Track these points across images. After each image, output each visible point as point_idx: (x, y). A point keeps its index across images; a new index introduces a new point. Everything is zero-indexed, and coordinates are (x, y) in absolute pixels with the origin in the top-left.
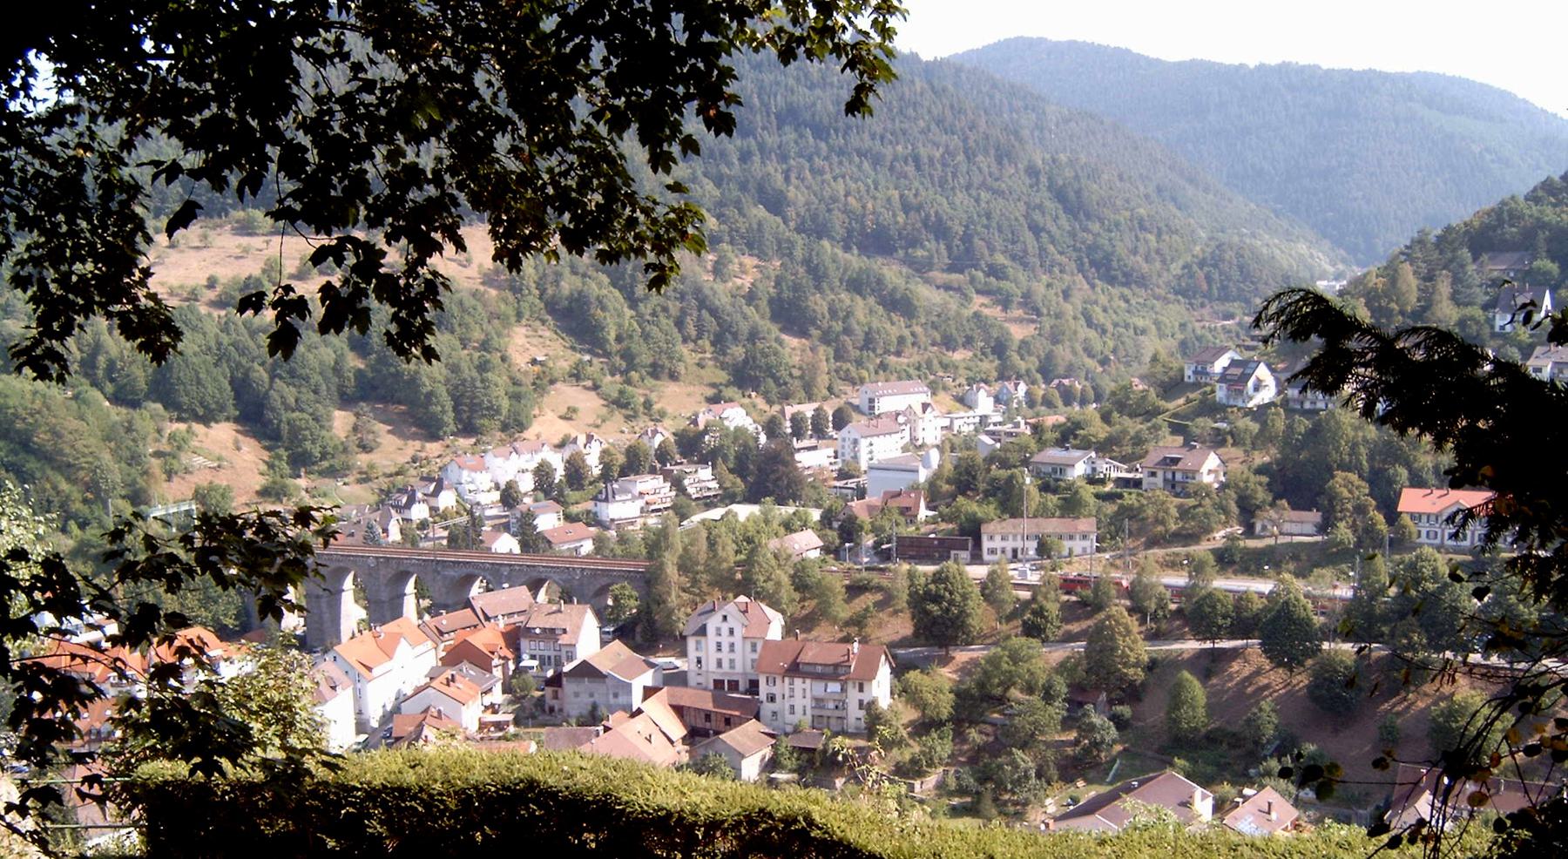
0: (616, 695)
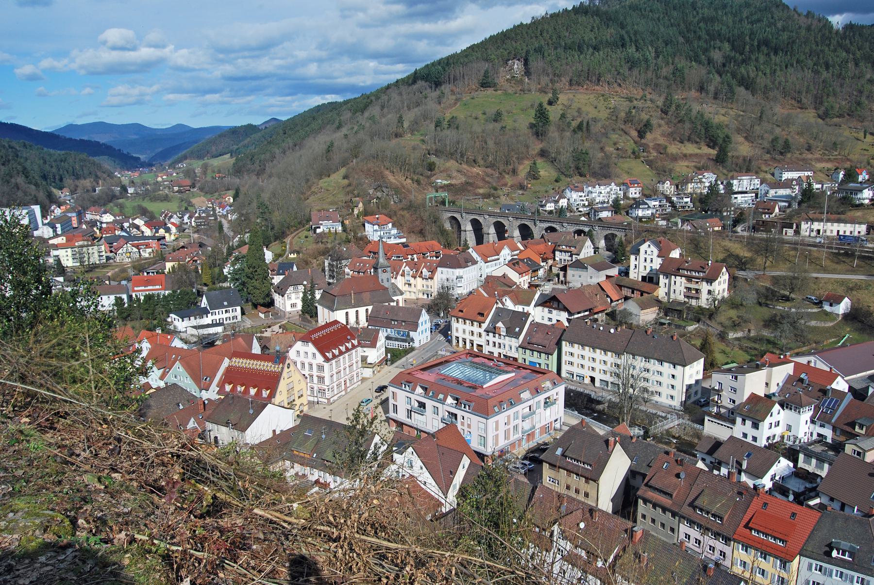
0: (591, 277)
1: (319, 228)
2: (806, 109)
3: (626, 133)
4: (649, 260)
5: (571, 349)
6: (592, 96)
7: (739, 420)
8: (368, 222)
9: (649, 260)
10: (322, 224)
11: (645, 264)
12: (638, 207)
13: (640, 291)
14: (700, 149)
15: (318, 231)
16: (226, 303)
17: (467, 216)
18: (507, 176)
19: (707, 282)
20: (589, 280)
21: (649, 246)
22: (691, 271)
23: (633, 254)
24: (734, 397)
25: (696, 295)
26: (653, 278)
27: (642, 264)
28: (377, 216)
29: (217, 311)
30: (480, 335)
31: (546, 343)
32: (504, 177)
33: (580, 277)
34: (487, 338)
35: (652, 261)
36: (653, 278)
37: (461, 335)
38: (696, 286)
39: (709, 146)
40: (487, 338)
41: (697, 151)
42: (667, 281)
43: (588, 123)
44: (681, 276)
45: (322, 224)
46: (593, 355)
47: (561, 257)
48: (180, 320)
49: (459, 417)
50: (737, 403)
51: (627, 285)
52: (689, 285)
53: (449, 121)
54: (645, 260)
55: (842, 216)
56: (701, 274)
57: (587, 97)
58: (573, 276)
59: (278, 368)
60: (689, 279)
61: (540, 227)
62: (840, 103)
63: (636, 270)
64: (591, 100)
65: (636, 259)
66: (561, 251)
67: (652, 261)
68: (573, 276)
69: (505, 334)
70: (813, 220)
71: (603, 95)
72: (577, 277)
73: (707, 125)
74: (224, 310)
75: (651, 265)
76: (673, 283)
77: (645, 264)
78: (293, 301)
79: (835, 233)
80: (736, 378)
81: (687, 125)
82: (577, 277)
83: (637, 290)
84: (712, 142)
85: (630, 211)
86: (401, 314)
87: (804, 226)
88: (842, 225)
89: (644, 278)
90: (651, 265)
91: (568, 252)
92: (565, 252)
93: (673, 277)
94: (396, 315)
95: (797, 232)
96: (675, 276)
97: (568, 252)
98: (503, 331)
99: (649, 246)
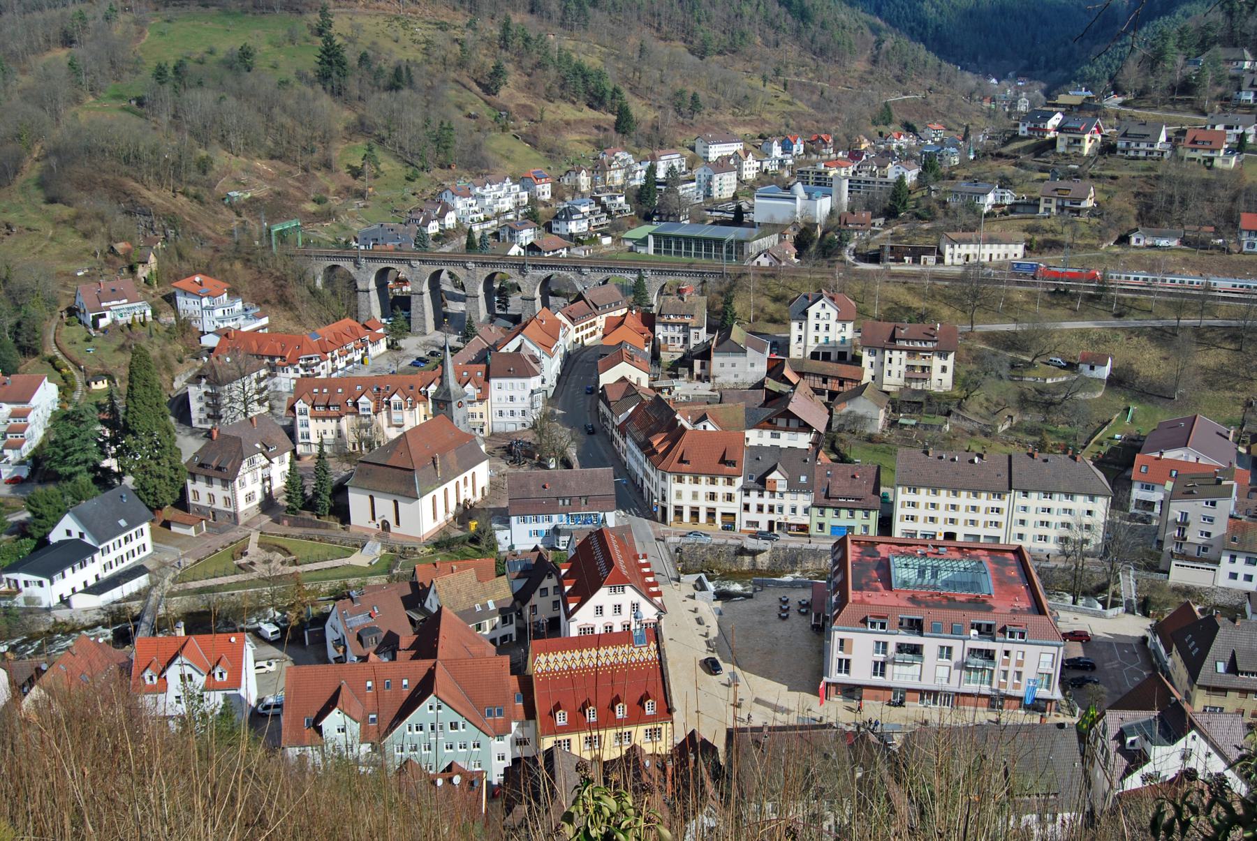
0: (752, 365)
1: (104, 316)
2: (672, 40)
3: (464, 86)
4: (822, 328)
5: (911, 497)
6: (380, 19)
7: (1225, 559)
8: (185, 293)
9: (822, 328)
10: (108, 309)
11: (817, 334)
12: (568, 220)
13: (837, 378)
14: (581, 111)
15: (103, 323)
16: (123, 523)
17: (371, 264)
18: (319, 174)
19: (940, 356)
20: (749, 369)
21: (823, 306)
22: (913, 341)
23: (797, 319)
24: (1207, 528)
25: (924, 376)
26: (829, 354)
27: (812, 333)
28: (197, 279)
29: (110, 543)
30: (730, 497)
31: (858, 493)
32: (314, 177)
33: (733, 365)
34: (746, 500)
35: (827, 328)
36: (829, 354)
37: (687, 503)
38: (924, 363)
39: (590, 106)
40: (746, 500)
41: (579, 115)
42: (873, 359)
43: (407, 69)
44: (901, 350)
45: (108, 309)
46: (934, 499)
47: (666, 334)
48: (46, 581)
49: (999, 656)
50: (1213, 536)
51: (814, 371)
52: (912, 362)
53: (175, 68)
54: (817, 328)
55: (972, 235)
56: (930, 345)
57: (374, 21)
58: (722, 365)
59: (649, 651)
60: (912, 353)
61: (533, 277)
62: (716, 36)
63: (801, 345)
64: (381, 26)
65: (800, 327)
66: (666, 324)
67: (827, 328)
68: (722, 365)
69: (784, 489)
70: (960, 242)
71: (397, 19)
72: (728, 367)
73: (581, 72)
74: (122, 537)
75: (827, 334)
76: (887, 361)
77: (817, 334)
78: (248, 490)
79: (986, 259)
80: (1213, 504)
81: (552, 72)
82: (728, 367)
83: (832, 377)
84: (596, 101)
85: (554, 226)
86: (573, 484)
87: (948, 250)
88: (995, 246)
89: (815, 355)
90: (827, 334)
91: (678, 324)
92: (673, 325)
93: (887, 352)
94: (565, 487)
95: (940, 260)
96: (891, 350)
97: (678, 324)
98: (782, 485)
99: (823, 306)
